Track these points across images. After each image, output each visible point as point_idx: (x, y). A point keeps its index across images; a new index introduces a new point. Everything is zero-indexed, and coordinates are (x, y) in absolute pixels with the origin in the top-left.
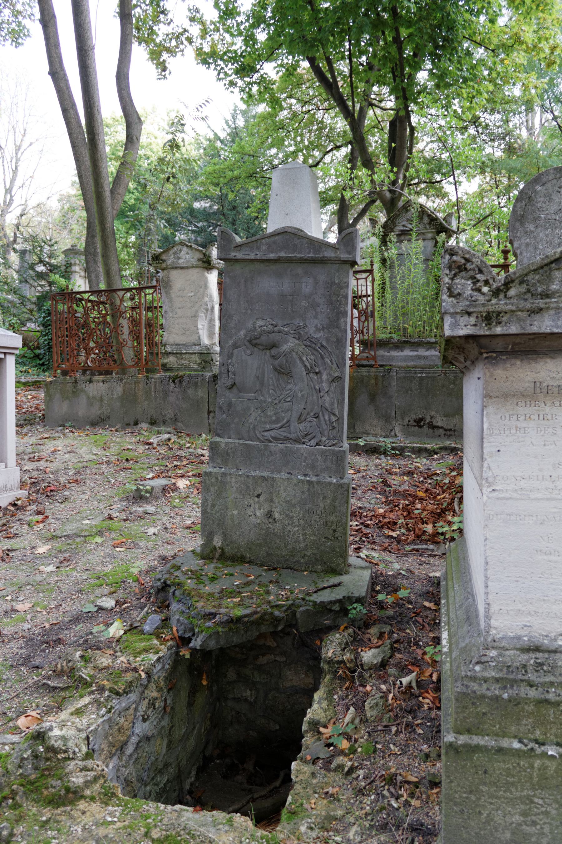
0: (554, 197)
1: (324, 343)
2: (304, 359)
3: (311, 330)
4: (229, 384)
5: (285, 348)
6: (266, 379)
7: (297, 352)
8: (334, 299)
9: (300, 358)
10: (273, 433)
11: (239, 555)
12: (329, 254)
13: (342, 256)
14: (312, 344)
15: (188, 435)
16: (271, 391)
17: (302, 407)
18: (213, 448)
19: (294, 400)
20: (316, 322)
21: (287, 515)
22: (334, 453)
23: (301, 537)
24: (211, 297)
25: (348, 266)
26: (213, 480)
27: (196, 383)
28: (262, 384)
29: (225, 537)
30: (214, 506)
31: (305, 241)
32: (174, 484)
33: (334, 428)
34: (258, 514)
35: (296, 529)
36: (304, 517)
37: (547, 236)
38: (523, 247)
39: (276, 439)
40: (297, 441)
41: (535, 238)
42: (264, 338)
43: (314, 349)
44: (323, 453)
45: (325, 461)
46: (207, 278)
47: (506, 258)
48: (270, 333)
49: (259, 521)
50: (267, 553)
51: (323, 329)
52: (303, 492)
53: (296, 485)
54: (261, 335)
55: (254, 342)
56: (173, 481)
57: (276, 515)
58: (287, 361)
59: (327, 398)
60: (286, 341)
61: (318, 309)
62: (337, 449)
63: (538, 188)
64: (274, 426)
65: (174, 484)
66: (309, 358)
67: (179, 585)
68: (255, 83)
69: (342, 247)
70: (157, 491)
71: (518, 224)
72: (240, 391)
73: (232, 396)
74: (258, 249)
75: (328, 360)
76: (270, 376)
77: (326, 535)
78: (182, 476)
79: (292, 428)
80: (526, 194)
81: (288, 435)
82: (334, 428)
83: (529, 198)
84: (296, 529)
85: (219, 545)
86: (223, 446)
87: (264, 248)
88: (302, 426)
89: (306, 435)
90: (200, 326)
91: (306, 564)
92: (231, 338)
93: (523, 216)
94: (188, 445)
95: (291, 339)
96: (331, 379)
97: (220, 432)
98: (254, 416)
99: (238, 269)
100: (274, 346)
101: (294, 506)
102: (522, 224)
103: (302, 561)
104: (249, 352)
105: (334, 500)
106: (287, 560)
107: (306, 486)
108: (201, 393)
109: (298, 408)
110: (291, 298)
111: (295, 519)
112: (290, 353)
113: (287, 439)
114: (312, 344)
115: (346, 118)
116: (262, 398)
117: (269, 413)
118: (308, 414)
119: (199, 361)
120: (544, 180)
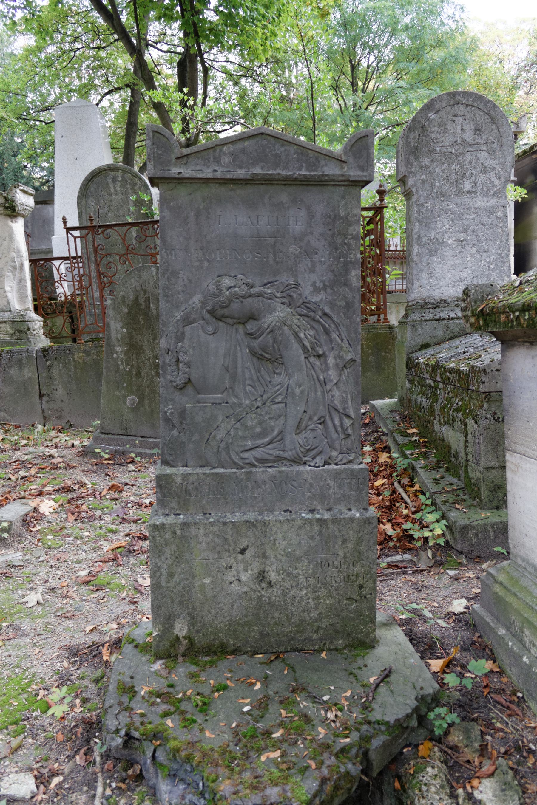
0: (449, 127)
1: (327, 310)
2: (302, 335)
4: (180, 380)
5: (269, 320)
6: (239, 370)
7: (290, 327)
8: (339, 241)
9: (296, 335)
11: (217, 643)
12: (332, 170)
13: (352, 173)
14: (308, 312)
15: (17, 427)
16: (248, 388)
18: (163, 484)
19: (289, 400)
20: (314, 277)
21: (289, 574)
23: (312, 603)
24: (19, 251)
26: (168, 536)
27: (20, 361)
28: (234, 377)
29: (192, 619)
30: (171, 575)
31: (292, 149)
32: (36, 510)
34: (244, 578)
35: (304, 592)
36: (315, 573)
37: (443, 171)
38: (419, 184)
39: (262, 461)
40: (296, 461)
41: (431, 173)
42: (235, 306)
43: (314, 320)
44: (336, 475)
45: (340, 487)
46: (11, 228)
47: (382, 200)
48: (244, 297)
49: (245, 589)
50: (261, 634)
51: (325, 288)
52: (312, 538)
53: (300, 528)
54: (231, 301)
55: (220, 312)
56: (33, 504)
57: (273, 576)
58: (275, 341)
59: (337, 393)
61: (316, 258)
62: (356, 467)
63: (432, 116)
64: (259, 442)
65: (36, 510)
66: (307, 335)
67: (157, 735)
68: (19, 8)
69: (351, 160)
70: (17, 527)
71: (412, 158)
73: (186, 401)
74: (217, 161)
75: (334, 335)
76: (245, 364)
77: (349, 595)
78: (41, 494)
79: (287, 443)
80: (419, 122)
81: (282, 453)
82: (348, 436)
83: (423, 127)
84: (304, 592)
85: (184, 633)
86: (179, 480)
87: (226, 159)
88: (300, 439)
89: (309, 450)
90: (7, 288)
91: (321, 639)
92: (178, 307)
93: (416, 148)
94: (24, 442)
96: (341, 365)
97: (170, 458)
98: (224, 428)
99: (182, 194)
100: (253, 317)
101: (299, 559)
102: (417, 158)
103: (315, 636)
104: (211, 329)
105: (358, 542)
106: (293, 639)
107: (316, 528)
108: (29, 372)
109: (295, 411)
110: (271, 241)
111: (302, 579)
112: (280, 328)
113: (279, 459)
114: (308, 312)
115: (131, 55)
116: (235, 400)
117: (249, 423)
118: (311, 418)
119: (11, 332)
120: (437, 107)
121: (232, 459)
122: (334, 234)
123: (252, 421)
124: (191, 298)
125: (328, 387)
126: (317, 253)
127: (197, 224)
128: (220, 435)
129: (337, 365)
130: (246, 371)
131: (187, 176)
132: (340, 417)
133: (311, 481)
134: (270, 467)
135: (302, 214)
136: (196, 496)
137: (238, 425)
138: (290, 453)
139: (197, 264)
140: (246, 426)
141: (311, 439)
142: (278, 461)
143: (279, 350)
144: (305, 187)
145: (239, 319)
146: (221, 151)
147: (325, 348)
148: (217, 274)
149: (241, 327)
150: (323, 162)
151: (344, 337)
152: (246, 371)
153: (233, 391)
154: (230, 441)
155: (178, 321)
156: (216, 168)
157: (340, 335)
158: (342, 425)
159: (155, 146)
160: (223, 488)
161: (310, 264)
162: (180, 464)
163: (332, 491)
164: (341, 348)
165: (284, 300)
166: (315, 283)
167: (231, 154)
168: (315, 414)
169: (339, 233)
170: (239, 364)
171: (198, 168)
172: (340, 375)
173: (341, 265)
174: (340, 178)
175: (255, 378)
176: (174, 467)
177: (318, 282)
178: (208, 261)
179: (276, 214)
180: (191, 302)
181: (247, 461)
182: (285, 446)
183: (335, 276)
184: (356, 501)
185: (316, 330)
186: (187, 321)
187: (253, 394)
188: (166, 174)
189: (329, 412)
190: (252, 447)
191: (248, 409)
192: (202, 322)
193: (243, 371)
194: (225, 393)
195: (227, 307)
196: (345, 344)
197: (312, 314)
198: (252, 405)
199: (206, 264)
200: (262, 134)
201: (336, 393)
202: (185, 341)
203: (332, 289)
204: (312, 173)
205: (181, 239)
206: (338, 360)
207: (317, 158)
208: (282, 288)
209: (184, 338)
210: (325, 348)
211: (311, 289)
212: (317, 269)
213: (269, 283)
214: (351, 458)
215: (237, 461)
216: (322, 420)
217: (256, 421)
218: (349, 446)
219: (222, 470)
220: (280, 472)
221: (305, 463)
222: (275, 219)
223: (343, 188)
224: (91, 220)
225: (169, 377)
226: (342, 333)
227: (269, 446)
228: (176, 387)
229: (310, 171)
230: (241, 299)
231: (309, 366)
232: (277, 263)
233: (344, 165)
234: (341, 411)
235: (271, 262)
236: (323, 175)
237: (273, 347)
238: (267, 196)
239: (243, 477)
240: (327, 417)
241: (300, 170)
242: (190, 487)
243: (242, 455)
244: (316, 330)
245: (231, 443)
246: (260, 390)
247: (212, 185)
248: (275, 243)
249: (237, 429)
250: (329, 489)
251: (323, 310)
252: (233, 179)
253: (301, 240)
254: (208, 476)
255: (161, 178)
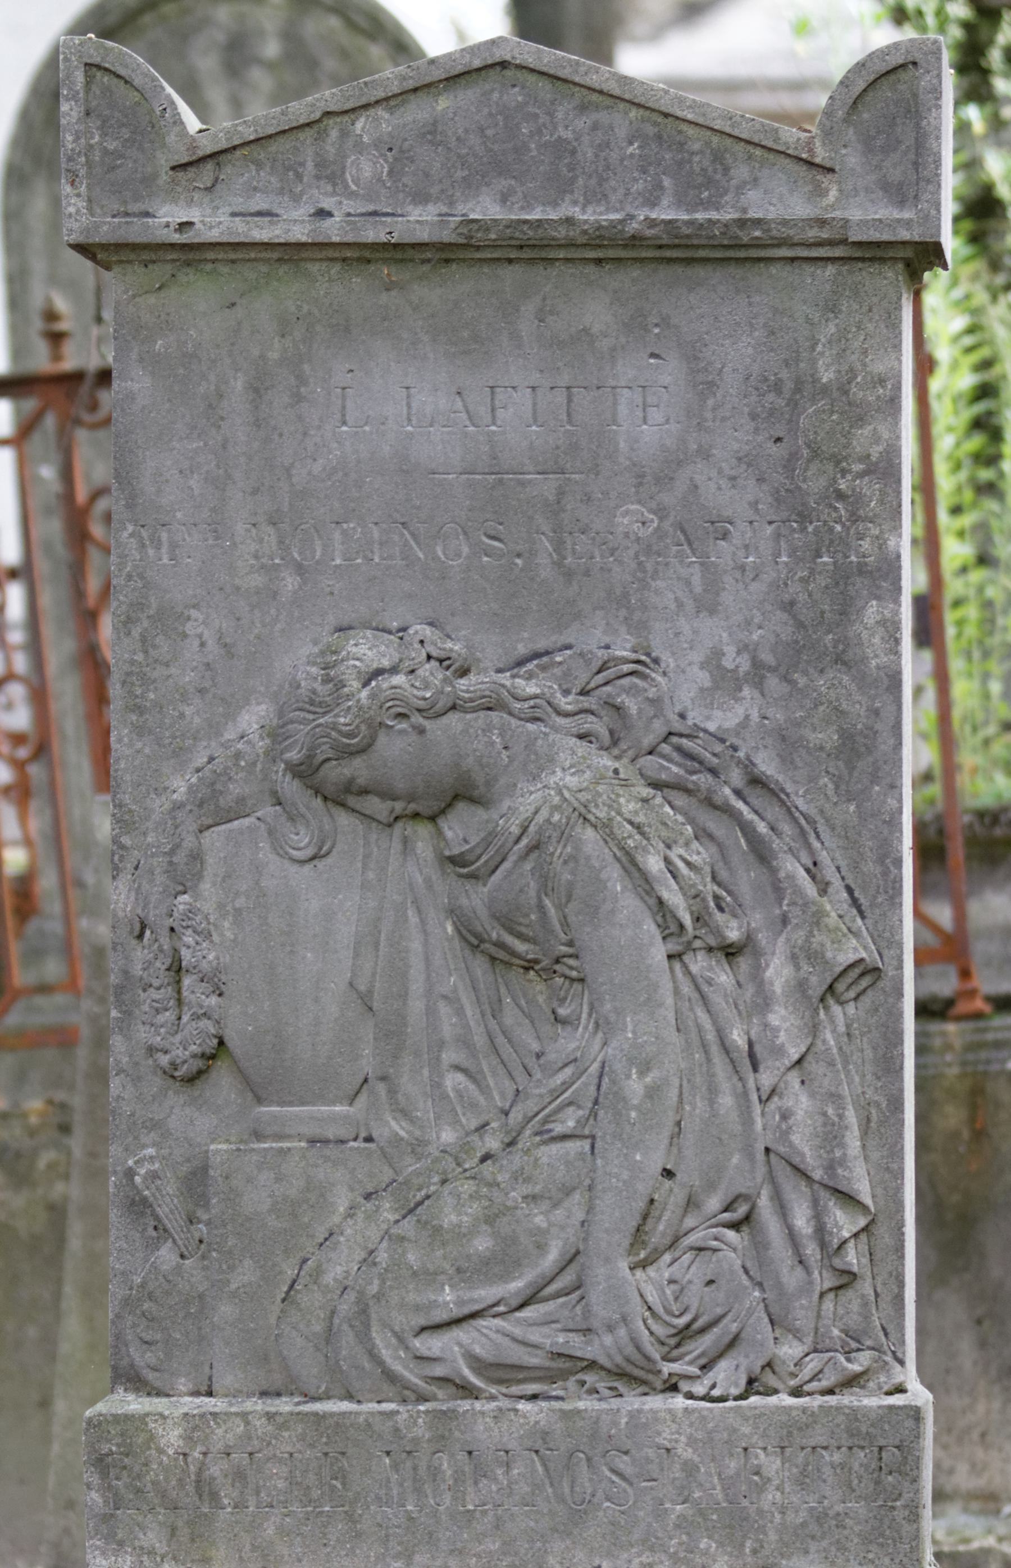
1: (767, 765)
2: (654, 864)
3: (683, 687)
4: (185, 1048)
5: (526, 803)
6: (416, 1006)
7: (605, 829)
8: (815, 483)
9: (631, 864)
10: (482, 1338)
12: (777, 201)
13: (855, 214)
14: (689, 771)
16: (453, 1081)
17: (656, 1162)
20: (714, 631)
22: (859, 1432)
25: (892, 275)
28: (393, 1036)
31: (622, 122)
33: (847, 1279)
39: (501, 1372)
40: (632, 1375)
42: (394, 748)
43: (710, 803)
44: (788, 1434)
45: (803, 1480)
48: (431, 711)
55: (336, 773)
58: (546, 883)
60: (537, 764)
61: (723, 554)
62: (872, 1401)
64: (486, 1294)
66: (679, 859)
69: (852, 159)
72: (257, 1092)
73: (204, 1126)
74: (331, 174)
75: (793, 868)
79: (596, 1296)
82: (847, 1279)
86: (172, 1438)
87: (364, 168)
88: (652, 1284)
89: (685, 1334)
92: (179, 754)
95: (571, 750)
96: (817, 985)
97: (141, 1358)
98: (353, 1242)
100: (463, 793)
104: (302, 840)
110: (547, 487)
112: (564, 834)
113: (566, 1367)
114: (689, 771)
116: (398, 1128)
117: (449, 1218)
118: (691, 1203)
121: (380, 1362)
122: (794, 456)
123: (459, 1208)
124: (231, 716)
125: (766, 1079)
126: (725, 536)
127: (257, 424)
128: (340, 1264)
129: (801, 986)
130: (444, 1009)
131: (213, 235)
132: (815, 1202)
133: (688, 1454)
134: (534, 1397)
135: (667, 380)
136: (239, 1505)
137: (408, 1227)
138: (608, 1340)
139: (257, 580)
140: (438, 1230)
141: (697, 1288)
142: (563, 1375)
143: (565, 923)
144: (679, 269)
145: (411, 798)
146: (344, 134)
147: (757, 919)
148: (332, 620)
149: (423, 830)
150: (741, 172)
151: (830, 873)
152: (444, 1009)
153: (392, 1092)
154: (374, 1288)
155: (178, 806)
156: (327, 204)
157: (813, 871)
158: (821, 1232)
159: (94, 123)
160: (341, 1475)
161: (697, 580)
162: (183, 1384)
163: (771, 1496)
164: (817, 918)
165: (590, 723)
166: (717, 654)
167: (387, 146)
168: (711, 1186)
169: (816, 454)
170: (417, 986)
171: (259, 202)
172: (814, 1030)
173: (822, 581)
174: (812, 233)
175: (480, 1040)
176: (159, 1394)
177: (730, 650)
178: (300, 569)
179: (565, 379)
180: (230, 734)
181: (439, 1371)
182: (587, 1313)
183: (800, 625)
184: (866, 1540)
185: (720, 846)
186: (213, 808)
187: (473, 1106)
188: (135, 232)
189: (771, 1178)
190: (457, 1312)
191: (449, 1163)
192: (268, 811)
193: (431, 1011)
194: (362, 1099)
195: (362, 750)
196: (835, 906)
197: (703, 780)
198: (466, 1148)
199: (290, 582)
200: (503, 65)
201: (800, 1102)
202: (205, 886)
203: (786, 679)
204: (700, 216)
205: (195, 482)
206: (806, 968)
207: (718, 157)
208: (582, 677)
209: (199, 876)
210: (757, 919)
211: (704, 678)
212: (727, 598)
213: (537, 655)
214: (856, 1368)
215: (398, 1368)
216: (742, 1210)
217: (474, 1208)
218: (854, 1320)
219: (346, 1406)
220: (566, 1415)
221: (674, 1388)
222: (560, 397)
223: (831, 270)
224: (56, 338)
225: (143, 1034)
226: (824, 857)
227: (527, 1313)
228: (170, 1073)
229: (692, 208)
230: (417, 719)
231: (687, 989)
232: (569, 575)
233: (825, 180)
234: (817, 1174)
235: (546, 571)
236: (742, 223)
237: (541, 907)
238: (529, 309)
239: (421, 1430)
240: (764, 1202)
241: (653, 204)
242: (215, 1470)
243: (421, 1344)
244: (720, 846)
245: (378, 1297)
246: (499, 1089)
247: (314, 268)
248: (561, 493)
249: (402, 1239)
250: (761, 1489)
251: (748, 765)
252: (385, 246)
253: (664, 480)
254: (284, 1426)
255: (119, 247)
